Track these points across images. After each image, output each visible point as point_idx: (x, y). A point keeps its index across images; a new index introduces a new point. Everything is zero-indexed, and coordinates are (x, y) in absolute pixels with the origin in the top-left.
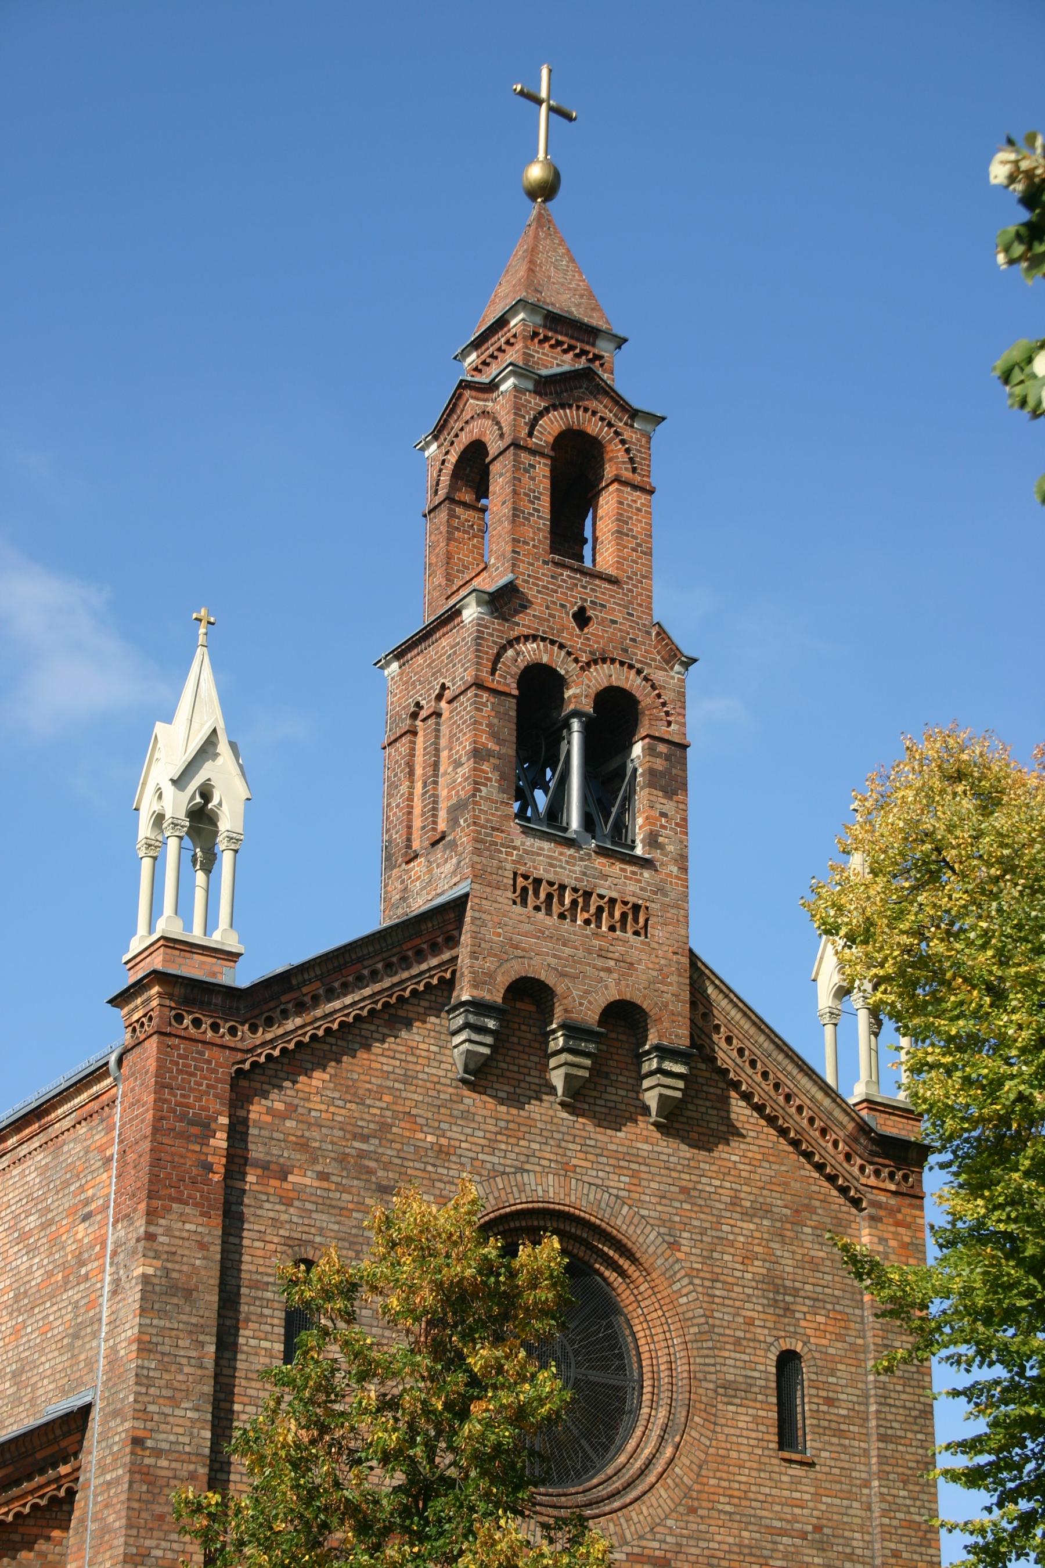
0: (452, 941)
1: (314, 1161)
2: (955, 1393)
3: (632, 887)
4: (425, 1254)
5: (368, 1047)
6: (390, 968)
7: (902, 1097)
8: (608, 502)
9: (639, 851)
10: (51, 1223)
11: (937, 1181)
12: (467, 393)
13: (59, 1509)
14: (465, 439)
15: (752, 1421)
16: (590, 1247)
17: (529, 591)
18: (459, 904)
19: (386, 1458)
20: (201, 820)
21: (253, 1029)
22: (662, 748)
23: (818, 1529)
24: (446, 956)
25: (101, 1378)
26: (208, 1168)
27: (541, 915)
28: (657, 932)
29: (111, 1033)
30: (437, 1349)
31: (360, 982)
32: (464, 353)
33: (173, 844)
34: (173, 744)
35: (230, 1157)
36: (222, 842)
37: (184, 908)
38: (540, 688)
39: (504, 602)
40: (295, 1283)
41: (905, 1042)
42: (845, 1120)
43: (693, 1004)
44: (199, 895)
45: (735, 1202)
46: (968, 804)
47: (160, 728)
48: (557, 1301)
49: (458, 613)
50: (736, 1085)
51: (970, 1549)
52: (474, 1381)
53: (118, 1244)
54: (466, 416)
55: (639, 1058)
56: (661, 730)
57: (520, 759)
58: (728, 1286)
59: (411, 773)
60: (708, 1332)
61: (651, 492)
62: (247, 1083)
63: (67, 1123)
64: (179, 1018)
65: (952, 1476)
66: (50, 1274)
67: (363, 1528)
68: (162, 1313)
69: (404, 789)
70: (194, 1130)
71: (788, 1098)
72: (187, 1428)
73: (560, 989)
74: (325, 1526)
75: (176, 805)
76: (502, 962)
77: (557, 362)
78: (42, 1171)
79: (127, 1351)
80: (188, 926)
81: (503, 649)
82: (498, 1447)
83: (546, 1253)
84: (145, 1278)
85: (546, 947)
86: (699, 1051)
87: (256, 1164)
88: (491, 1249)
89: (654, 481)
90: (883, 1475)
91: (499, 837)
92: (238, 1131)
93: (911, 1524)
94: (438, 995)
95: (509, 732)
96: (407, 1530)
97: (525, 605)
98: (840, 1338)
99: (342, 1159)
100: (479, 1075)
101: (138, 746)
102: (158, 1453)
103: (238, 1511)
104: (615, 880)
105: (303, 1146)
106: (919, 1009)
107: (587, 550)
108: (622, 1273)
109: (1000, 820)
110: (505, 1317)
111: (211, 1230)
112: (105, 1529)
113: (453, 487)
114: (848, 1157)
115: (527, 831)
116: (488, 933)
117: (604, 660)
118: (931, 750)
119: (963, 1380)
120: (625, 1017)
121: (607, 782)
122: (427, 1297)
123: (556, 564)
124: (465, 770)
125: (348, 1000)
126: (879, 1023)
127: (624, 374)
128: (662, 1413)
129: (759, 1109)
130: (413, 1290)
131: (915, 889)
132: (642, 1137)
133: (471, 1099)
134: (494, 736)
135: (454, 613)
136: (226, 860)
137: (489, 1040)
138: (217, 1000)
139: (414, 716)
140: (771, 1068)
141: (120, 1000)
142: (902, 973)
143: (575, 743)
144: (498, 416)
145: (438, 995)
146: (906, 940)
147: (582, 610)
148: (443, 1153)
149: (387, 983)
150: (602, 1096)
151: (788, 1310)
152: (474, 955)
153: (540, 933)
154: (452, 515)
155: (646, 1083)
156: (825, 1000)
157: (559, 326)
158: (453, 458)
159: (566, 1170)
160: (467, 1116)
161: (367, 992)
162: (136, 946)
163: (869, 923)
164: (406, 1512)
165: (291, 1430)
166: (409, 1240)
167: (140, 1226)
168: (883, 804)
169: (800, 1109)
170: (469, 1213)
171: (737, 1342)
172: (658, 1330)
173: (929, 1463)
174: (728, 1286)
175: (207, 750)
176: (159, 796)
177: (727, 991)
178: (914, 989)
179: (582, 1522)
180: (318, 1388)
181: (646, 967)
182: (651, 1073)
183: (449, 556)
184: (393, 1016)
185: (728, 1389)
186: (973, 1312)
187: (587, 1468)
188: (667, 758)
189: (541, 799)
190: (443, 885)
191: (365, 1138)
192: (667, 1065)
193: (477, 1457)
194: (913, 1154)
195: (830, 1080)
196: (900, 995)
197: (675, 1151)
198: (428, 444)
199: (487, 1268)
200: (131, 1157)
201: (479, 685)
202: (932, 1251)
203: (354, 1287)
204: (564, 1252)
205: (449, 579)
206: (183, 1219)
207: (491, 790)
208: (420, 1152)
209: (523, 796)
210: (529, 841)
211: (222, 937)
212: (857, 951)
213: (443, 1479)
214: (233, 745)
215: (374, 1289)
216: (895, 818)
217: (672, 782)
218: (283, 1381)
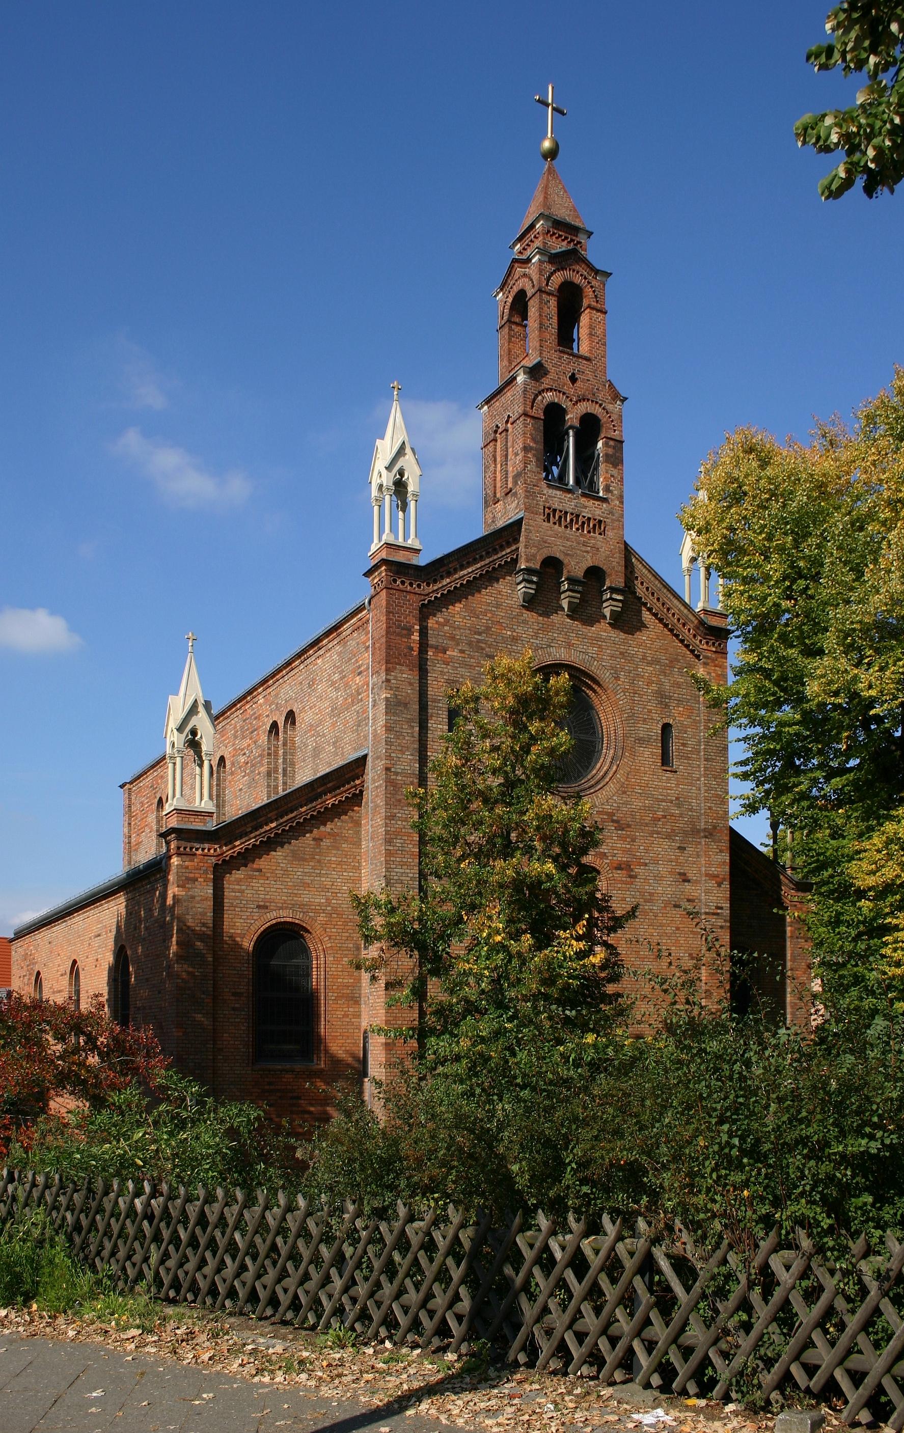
0: (516, 541)
1: (458, 644)
2: (739, 740)
3: (598, 512)
4: (510, 682)
5: (479, 592)
6: (488, 554)
7: (719, 607)
8: (584, 319)
9: (601, 494)
10: (344, 677)
11: (734, 646)
12: (516, 265)
13: (357, 799)
14: (516, 289)
15: (650, 754)
16: (581, 679)
17: (548, 366)
18: (519, 522)
19: (494, 772)
20: (400, 486)
21: (428, 585)
22: (612, 443)
23: (677, 799)
24: (514, 548)
25: (371, 743)
26: (412, 649)
27: (557, 526)
28: (610, 534)
29: (364, 590)
30: (515, 724)
31: (475, 561)
32: (514, 245)
33: (387, 498)
34: (385, 449)
35: (421, 644)
36: (410, 497)
37: (394, 529)
38: (554, 413)
39: (536, 372)
40: (453, 697)
41: (721, 581)
42: (693, 619)
43: (626, 567)
44: (401, 523)
45: (644, 658)
46: (755, 464)
47: (378, 442)
48: (567, 704)
49: (515, 378)
50: (645, 604)
51: (743, 806)
52: (532, 737)
53: (374, 685)
54: (516, 277)
55: (601, 593)
56: (611, 434)
57: (546, 451)
58: (641, 696)
59: (495, 460)
60: (632, 716)
61: (605, 313)
62: (427, 610)
63: (348, 632)
64: (395, 581)
65: (736, 776)
66: (346, 699)
67: (486, 801)
68: (395, 714)
69: (492, 468)
70: (404, 632)
71: (668, 609)
72: (408, 763)
73: (566, 561)
74: (469, 801)
75: (387, 479)
76: (539, 549)
77: (559, 246)
78: (339, 654)
79: (381, 731)
80: (397, 538)
81: (536, 396)
82: (542, 766)
83: (562, 680)
84: (387, 699)
86: (628, 589)
87: (432, 647)
88: (538, 679)
89: (607, 307)
90: (706, 775)
92: (423, 632)
93: (717, 796)
94: (511, 566)
95: (540, 437)
96: (505, 802)
97: (546, 373)
98: (689, 717)
99: (470, 644)
100: (530, 603)
101: (369, 453)
102: (397, 774)
103: (432, 795)
104: (591, 509)
105: (452, 638)
106: (729, 564)
107: (575, 345)
108: (594, 691)
109: (769, 471)
110: (545, 709)
111: (414, 677)
112: (377, 806)
113: (510, 315)
114: (695, 636)
115: (549, 486)
116: (533, 536)
118: (737, 438)
119: (743, 734)
120: (595, 574)
121: (586, 462)
122: (510, 701)
123: (561, 352)
124: (520, 457)
125: (470, 570)
126: (710, 574)
127: (593, 251)
128: (612, 751)
129: (655, 615)
130: (505, 698)
131: (729, 507)
132: (602, 629)
133: (527, 614)
134: (533, 439)
135: (514, 379)
136: (412, 505)
137: (534, 586)
138: (411, 572)
139: (496, 432)
140: (661, 596)
141: (368, 574)
142: (721, 548)
143: (569, 441)
144: (531, 277)
145: (511, 566)
146: (725, 531)
147: (573, 374)
148: (515, 639)
149: (487, 561)
150: (585, 612)
152: (526, 547)
153: (556, 535)
154: (510, 329)
155: (605, 605)
156: (685, 564)
157: (561, 227)
158: (510, 300)
159: (569, 645)
160: (525, 622)
161: (479, 565)
162: (374, 548)
163: (708, 523)
164: (503, 794)
165: (454, 760)
166: (503, 675)
167: (383, 676)
168: (715, 465)
169: (673, 615)
170: (529, 663)
171: (645, 720)
172: (609, 716)
173: (726, 771)
174: (641, 696)
175: (401, 452)
176: (380, 475)
177: (641, 560)
178: (728, 555)
179: (580, 797)
180: (465, 742)
181: (604, 550)
182: (607, 600)
183: (510, 351)
184: (490, 577)
185: (640, 741)
186: (750, 705)
187: (579, 776)
188: (614, 448)
189: (556, 471)
190: (511, 514)
191: (480, 634)
192: (614, 596)
193: (533, 770)
194: (723, 634)
195: (687, 601)
196: (720, 559)
197: (617, 636)
198: (498, 293)
199: (536, 687)
200: (377, 645)
201: (525, 414)
202: (731, 678)
203: (478, 699)
204: (570, 680)
205: (510, 362)
206: (402, 672)
207: (532, 467)
208: (505, 640)
209: (548, 470)
210: (550, 491)
211: (412, 542)
212: (701, 539)
213: (519, 780)
214: (412, 449)
215: (487, 698)
216: (720, 473)
217: (616, 460)
218: (449, 740)
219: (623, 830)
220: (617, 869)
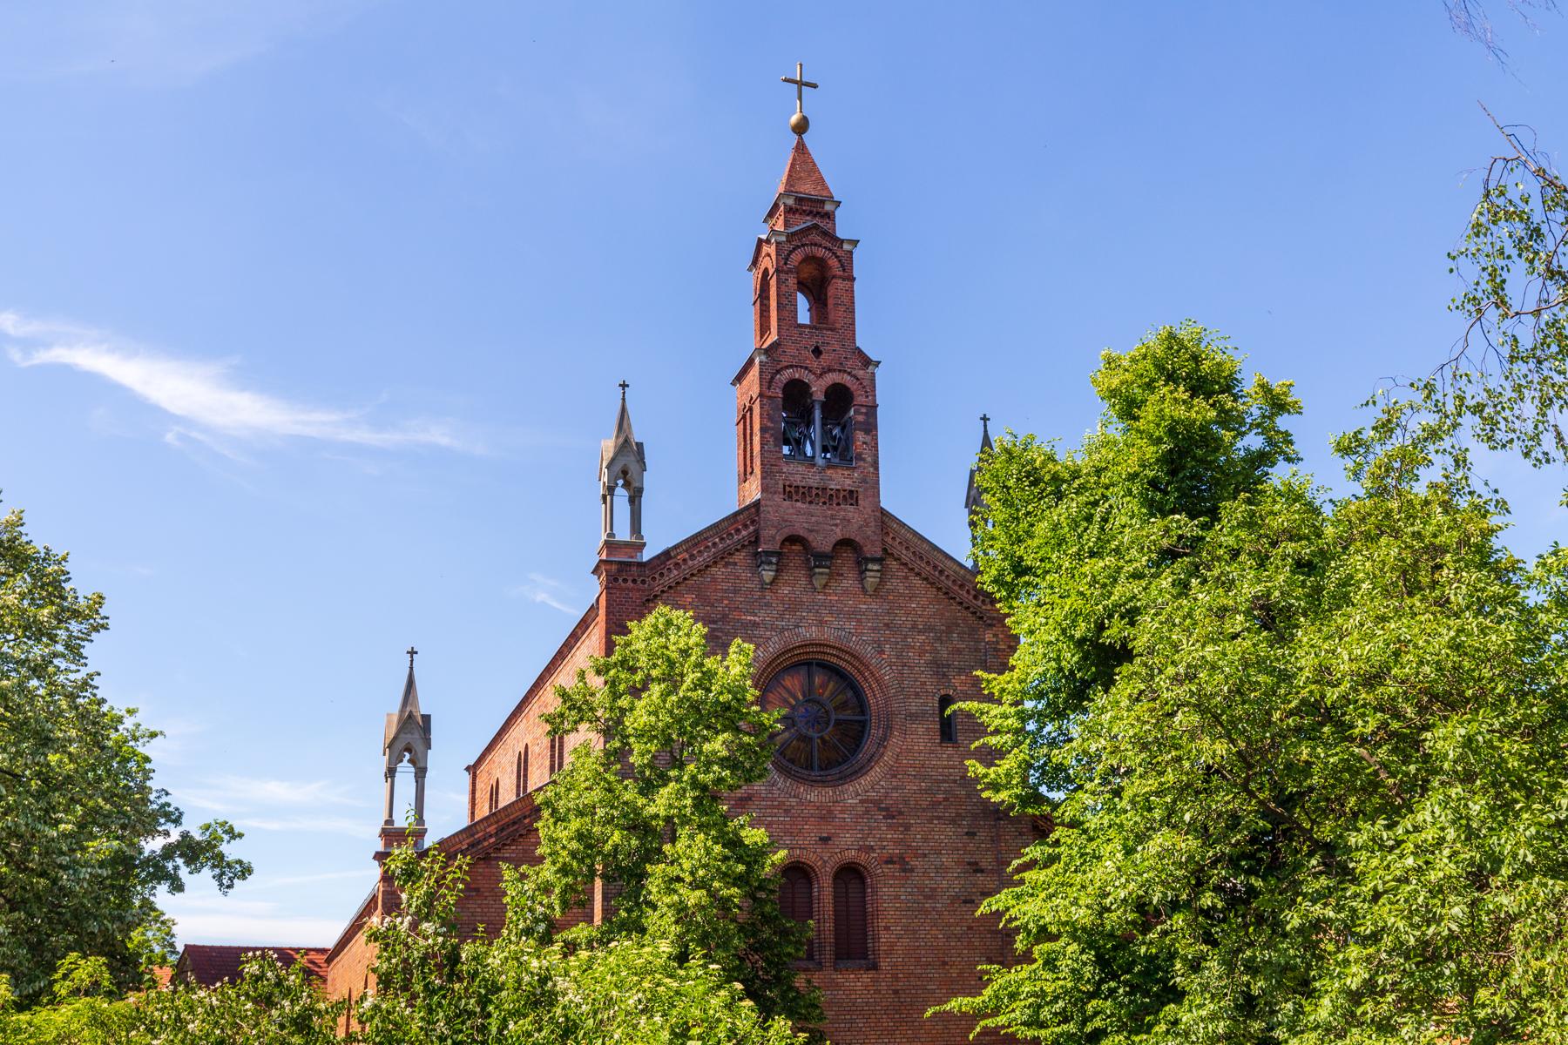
3: (848, 482)
45: (914, 626)
85: (802, 518)
91: (775, 469)
104: (840, 479)
151: (944, 675)
153: (798, 513)
159: (822, 623)
171: (917, 694)
185: (913, 717)
217: (871, 427)
219: (893, 817)
220: (887, 862)
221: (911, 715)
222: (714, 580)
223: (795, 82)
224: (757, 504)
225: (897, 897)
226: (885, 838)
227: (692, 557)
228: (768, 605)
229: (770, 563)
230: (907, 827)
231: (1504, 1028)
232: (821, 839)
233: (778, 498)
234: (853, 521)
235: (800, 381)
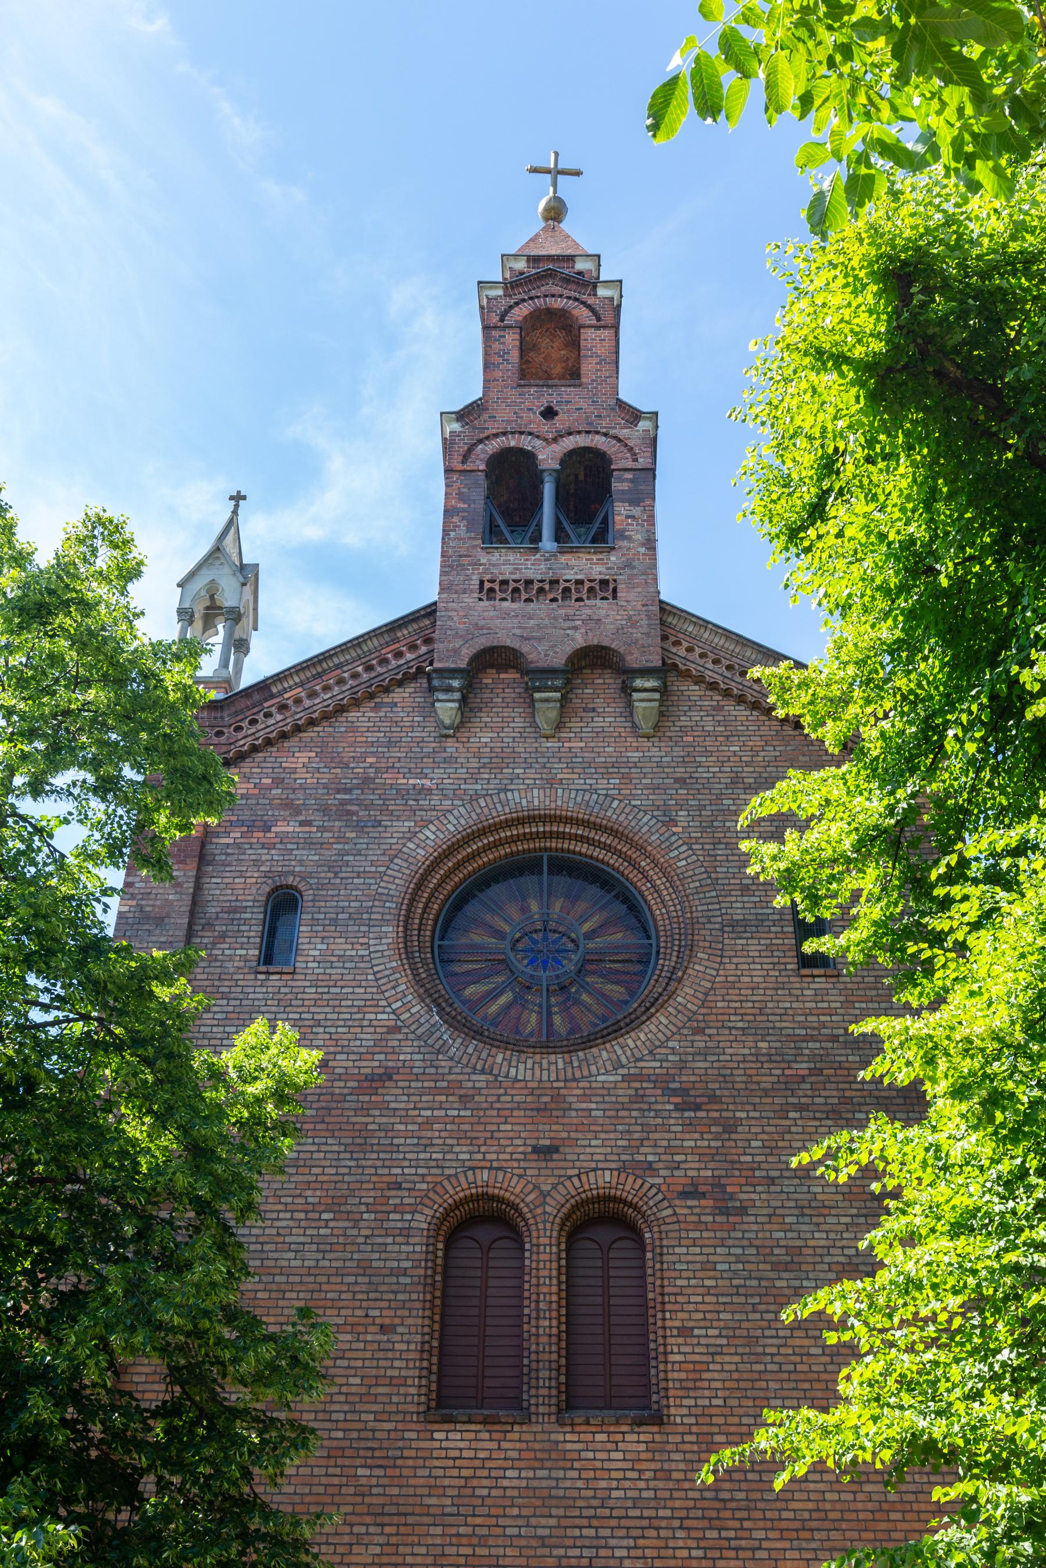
3: (599, 568)
91: (466, 561)
99: (325, 810)
117: (570, 434)
159: (551, 783)
219: (698, 1107)
220: (684, 1195)
221: (734, 924)
222: (352, 729)
223: (548, 171)
224: (430, 611)
225: (709, 1266)
226: (682, 1150)
227: (313, 694)
228: (449, 760)
229: (449, 689)
230: (730, 1127)
231: (3, 1559)
232: (536, 1150)
233: (470, 599)
234: (607, 622)
235: (521, 451)
